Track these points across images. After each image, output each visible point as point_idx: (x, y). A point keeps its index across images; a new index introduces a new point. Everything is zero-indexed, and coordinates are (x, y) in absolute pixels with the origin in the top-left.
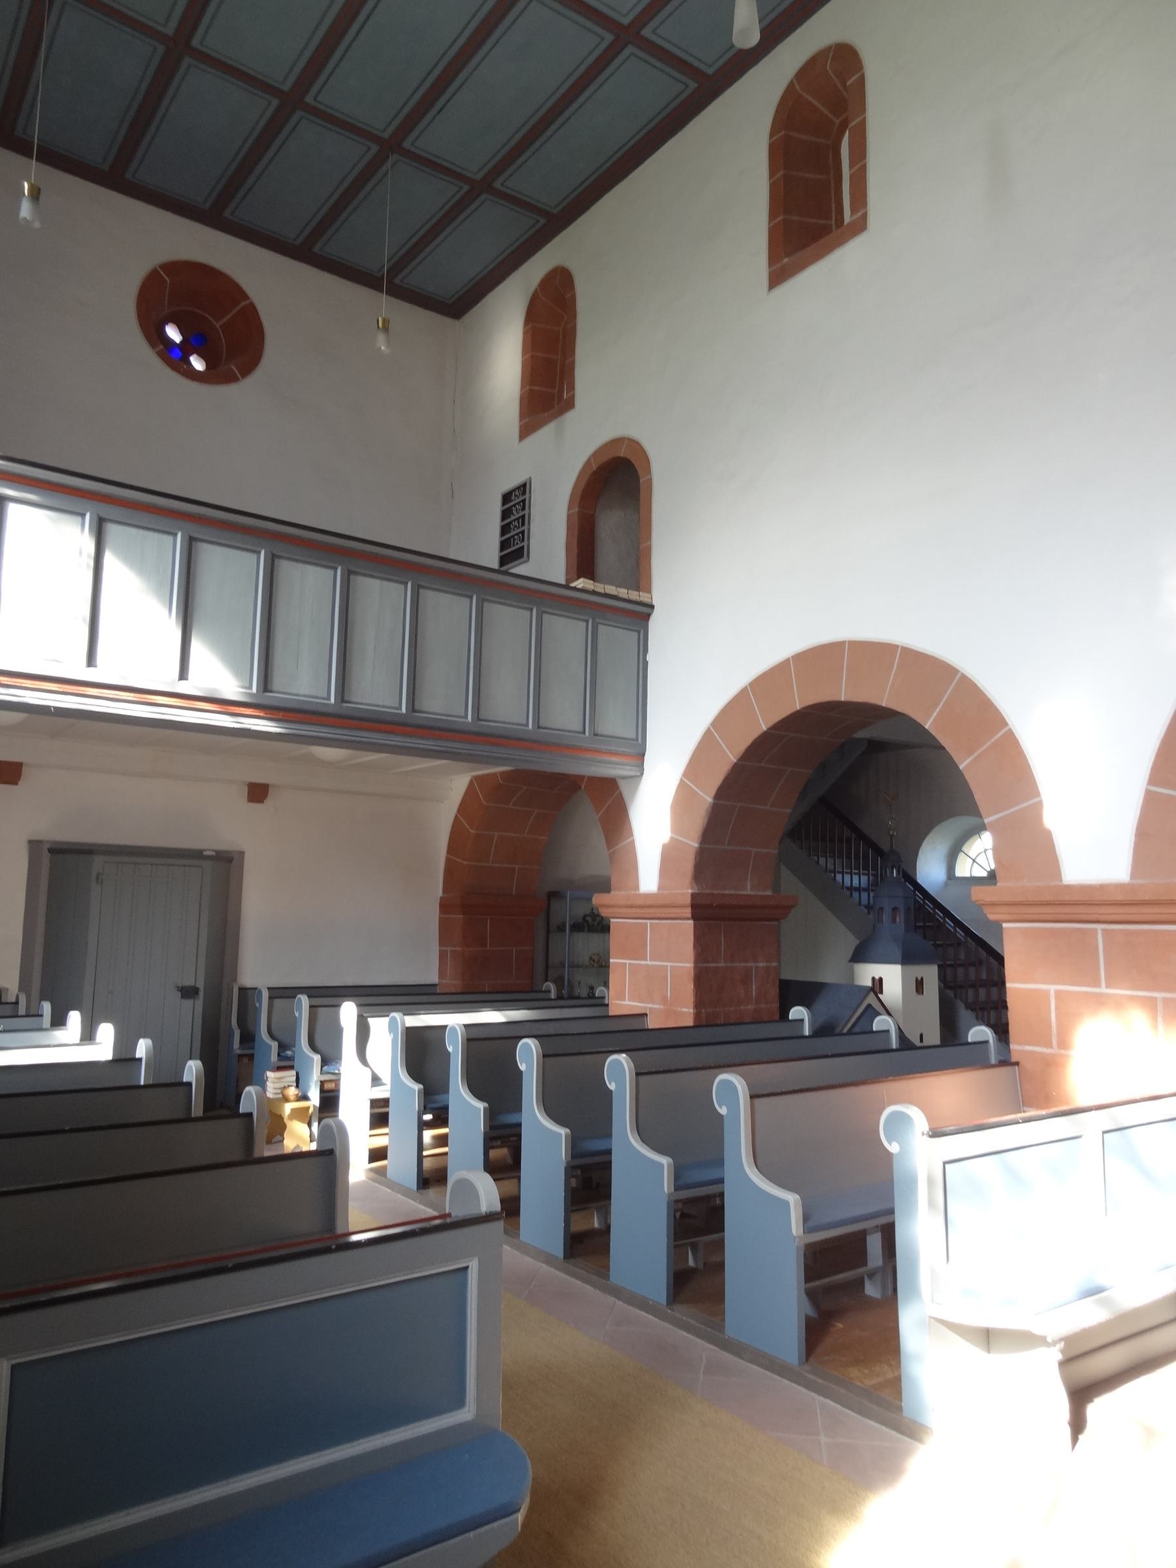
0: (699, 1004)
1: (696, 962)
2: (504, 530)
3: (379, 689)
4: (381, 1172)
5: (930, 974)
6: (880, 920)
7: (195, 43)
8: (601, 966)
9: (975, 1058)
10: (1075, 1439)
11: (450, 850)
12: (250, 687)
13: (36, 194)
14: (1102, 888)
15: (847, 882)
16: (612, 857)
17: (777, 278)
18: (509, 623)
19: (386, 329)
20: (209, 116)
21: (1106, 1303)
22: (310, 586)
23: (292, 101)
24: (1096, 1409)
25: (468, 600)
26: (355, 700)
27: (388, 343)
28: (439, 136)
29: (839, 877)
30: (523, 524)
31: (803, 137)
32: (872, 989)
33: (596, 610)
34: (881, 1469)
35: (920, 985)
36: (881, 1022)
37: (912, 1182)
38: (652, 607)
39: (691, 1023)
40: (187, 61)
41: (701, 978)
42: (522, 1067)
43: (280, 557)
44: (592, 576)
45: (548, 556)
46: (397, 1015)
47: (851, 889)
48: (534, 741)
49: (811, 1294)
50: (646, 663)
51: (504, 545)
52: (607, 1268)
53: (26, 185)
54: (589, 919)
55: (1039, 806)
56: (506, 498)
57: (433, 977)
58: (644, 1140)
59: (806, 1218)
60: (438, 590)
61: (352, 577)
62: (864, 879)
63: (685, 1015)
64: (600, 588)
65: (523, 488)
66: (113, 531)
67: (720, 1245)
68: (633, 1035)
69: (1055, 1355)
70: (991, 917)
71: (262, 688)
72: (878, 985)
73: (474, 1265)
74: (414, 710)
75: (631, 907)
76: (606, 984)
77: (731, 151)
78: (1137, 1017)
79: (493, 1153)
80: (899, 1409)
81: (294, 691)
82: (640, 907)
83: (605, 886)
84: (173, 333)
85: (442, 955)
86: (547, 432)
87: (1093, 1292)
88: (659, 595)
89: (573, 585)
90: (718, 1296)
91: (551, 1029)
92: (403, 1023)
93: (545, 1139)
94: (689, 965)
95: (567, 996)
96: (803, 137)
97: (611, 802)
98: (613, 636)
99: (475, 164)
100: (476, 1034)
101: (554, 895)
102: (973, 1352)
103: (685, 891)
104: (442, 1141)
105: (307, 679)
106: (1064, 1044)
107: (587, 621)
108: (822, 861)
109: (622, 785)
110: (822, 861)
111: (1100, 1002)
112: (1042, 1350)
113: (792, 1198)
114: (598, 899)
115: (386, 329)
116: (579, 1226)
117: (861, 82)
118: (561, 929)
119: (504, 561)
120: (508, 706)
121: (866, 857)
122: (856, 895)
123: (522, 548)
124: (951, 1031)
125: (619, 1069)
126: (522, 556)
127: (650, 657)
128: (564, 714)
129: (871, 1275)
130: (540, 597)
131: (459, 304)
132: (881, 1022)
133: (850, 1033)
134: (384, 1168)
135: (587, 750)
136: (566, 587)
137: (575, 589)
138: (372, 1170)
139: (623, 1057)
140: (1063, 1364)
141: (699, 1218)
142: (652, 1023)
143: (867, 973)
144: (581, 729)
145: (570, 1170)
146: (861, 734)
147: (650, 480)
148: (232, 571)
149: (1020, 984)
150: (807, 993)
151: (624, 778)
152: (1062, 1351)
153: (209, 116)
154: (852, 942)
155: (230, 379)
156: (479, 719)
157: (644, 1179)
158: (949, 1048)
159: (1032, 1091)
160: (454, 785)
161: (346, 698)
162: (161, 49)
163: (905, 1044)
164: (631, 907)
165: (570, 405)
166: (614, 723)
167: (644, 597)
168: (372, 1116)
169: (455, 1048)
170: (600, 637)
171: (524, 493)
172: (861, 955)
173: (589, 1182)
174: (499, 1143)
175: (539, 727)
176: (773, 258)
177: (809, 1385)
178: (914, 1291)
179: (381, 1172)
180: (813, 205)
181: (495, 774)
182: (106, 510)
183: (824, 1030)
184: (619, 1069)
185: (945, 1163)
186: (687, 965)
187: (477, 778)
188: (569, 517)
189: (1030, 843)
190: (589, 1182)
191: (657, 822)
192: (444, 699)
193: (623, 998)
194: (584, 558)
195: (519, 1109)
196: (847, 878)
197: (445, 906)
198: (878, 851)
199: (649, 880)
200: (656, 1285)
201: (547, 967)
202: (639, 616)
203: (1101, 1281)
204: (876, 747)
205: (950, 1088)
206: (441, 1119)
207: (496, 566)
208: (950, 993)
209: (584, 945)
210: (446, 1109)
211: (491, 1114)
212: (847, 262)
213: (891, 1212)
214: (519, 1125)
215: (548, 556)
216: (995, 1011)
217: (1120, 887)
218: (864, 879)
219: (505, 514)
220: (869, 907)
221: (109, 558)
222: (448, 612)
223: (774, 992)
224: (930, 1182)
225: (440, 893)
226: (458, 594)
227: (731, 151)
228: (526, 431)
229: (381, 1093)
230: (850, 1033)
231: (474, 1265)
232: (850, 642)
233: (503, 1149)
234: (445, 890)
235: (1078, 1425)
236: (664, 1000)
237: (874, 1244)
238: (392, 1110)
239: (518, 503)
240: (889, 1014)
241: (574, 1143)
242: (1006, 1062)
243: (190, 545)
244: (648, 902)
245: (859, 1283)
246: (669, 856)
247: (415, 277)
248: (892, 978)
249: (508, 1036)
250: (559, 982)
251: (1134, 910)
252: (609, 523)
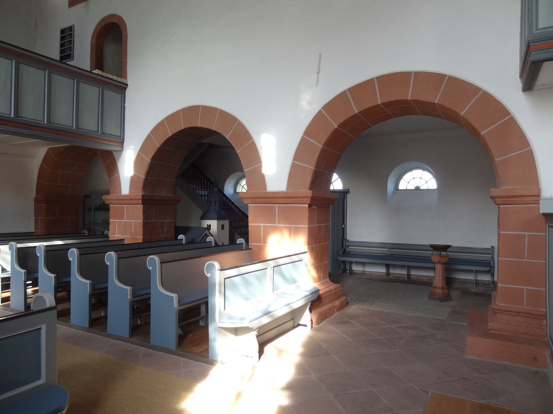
0: (144, 235)
1: (143, 220)
2: (62, 45)
4: (8, 306)
5: (226, 223)
6: (211, 205)
8: (107, 224)
9: (239, 248)
10: (260, 357)
11: (39, 177)
14: (278, 193)
15: (200, 193)
16: (110, 181)
18: (64, 85)
21: (270, 316)
24: (267, 348)
29: (198, 191)
30: (71, 44)
31: (513, 154)
32: (207, 228)
33: (103, 84)
34: (202, 375)
35: (223, 227)
36: (209, 239)
37: (214, 285)
38: (127, 85)
39: (139, 238)
41: (145, 226)
42: (71, 259)
44: (102, 70)
45: (82, 57)
46: (13, 243)
47: (201, 195)
49: (181, 327)
50: (124, 107)
51: (62, 52)
52: (106, 328)
54: (102, 206)
55: (261, 166)
57: (32, 229)
58: (121, 281)
59: (179, 302)
60: (29, 65)
62: (206, 192)
63: (139, 238)
64: (105, 74)
65: (71, 28)
67: (149, 316)
68: (119, 246)
69: (254, 333)
70: (245, 202)
72: (209, 227)
73: (44, 327)
74: (18, 116)
75: (118, 200)
76: (109, 230)
78: (286, 233)
79: (59, 295)
80: (208, 357)
82: (121, 200)
83: (108, 193)
85: (36, 221)
87: (267, 313)
88: (130, 80)
89: (93, 72)
90: (148, 332)
91: (85, 245)
92: (16, 246)
93: (80, 285)
94: (141, 221)
95: (92, 234)
96: (513, 154)
97: (110, 161)
98: (111, 96)
100: (49, 249)
101: (86, 197)
102: (231, 336)
103: (139, 194)
104: (36, 292)
106: (265, 242)
108: (192, 186)
109: (114, 153)
110: (192, 186)
111: (275, 229)
112: (252, 332)
113: (174, 296)
114: (104, 197)
116: (96, 315)
118: (90, 210)
119: (62, 58)
120: (63, 117)
121: (207, 185)
122: (203, 197)
124: (232, 241)
125: (111, 258)
126: (70, 58)
128: (89, 123)
129: (202, 319)
130: (77, 74)
132: (209, 239)
133: (199, 242)
134: (9, 304)
135: (100, 139)
136: (90, 72)
137: (94, 73)
138: (2, 306)
139: (112, 253)
140: (258, 336)
141: (141, 308)
142: (126, 242)
143: (206, 223)
145: (91, 296)
146: (205, 141)
147: (127, 34)
149: (252, 224)
150: (184, 230)
151: (116, 151)
152: (258, 332)
154: (202, 213)
157: (120, 293)
158: (232, 245)
159: (255, 256)
160: (39, 152)
163: (217, 245)
164: (118, 200)
166: (111, 129)
167: (123, 81)
168: (2, 285)
169: (41, 255)
170: (105, 95)
171: (71, 31)
172: (204, 217)
173: (99, 299)
174: (61, 289)
177: (179, 355)
178: (214, 320)
179: (8, 306)
181: (59, 147)
183: (190, 242)
184: (111, 258)
185: (225, 279)
186: (140, 221)
187: (50, 148)
188: (92, 44)
189: (258, 179)
190: (99, 299)
191: (128, 166)
192: (33, 111)
193: (115, 234)
194: (98, 61)
195: (69, 276)
196: (200, 192)
197: (37, 201)
198: (211, 183)
199: (125, 190)
200: (125, 331)
201: (84, 224)
202: (122, 88)
203: (270, 309)
204: (211, 146)
205: (230, 257)
206: (35, 283)
207: (58, 59)
208: (233, 230)
209: (100, 216)
210: (37, 278)
211: (57, 279)
213: (207, 297)
214: (70, 282)
215: (82, 57)
216: (245, 235)
217: (283, 192)
218: (206, 192)
219: (62, 39)
220: (207, 202)
222: (34, 77)
223: (173, 230)
224: (220, 284)
225: (34, 195)
226: (40, 69)
229: (5, 275)
230: (199, 242)
231: (44, 327)
232: (202, 106)
233: (63, 288)
234: (37, 193)
235: (261, 352)
236: (131, 234)
237: (203, 307)
238: (12, 283)
239: (68, 35)
240: (212, 236)
241: (93, 286)
242: (248, 249)
244: (125, 198)
245: (198, 322)
246: (133, 180)
248: (214, 224)
249: (65, 249)
250: (89, 230)
251: (287, 200)
252: (109, 50)
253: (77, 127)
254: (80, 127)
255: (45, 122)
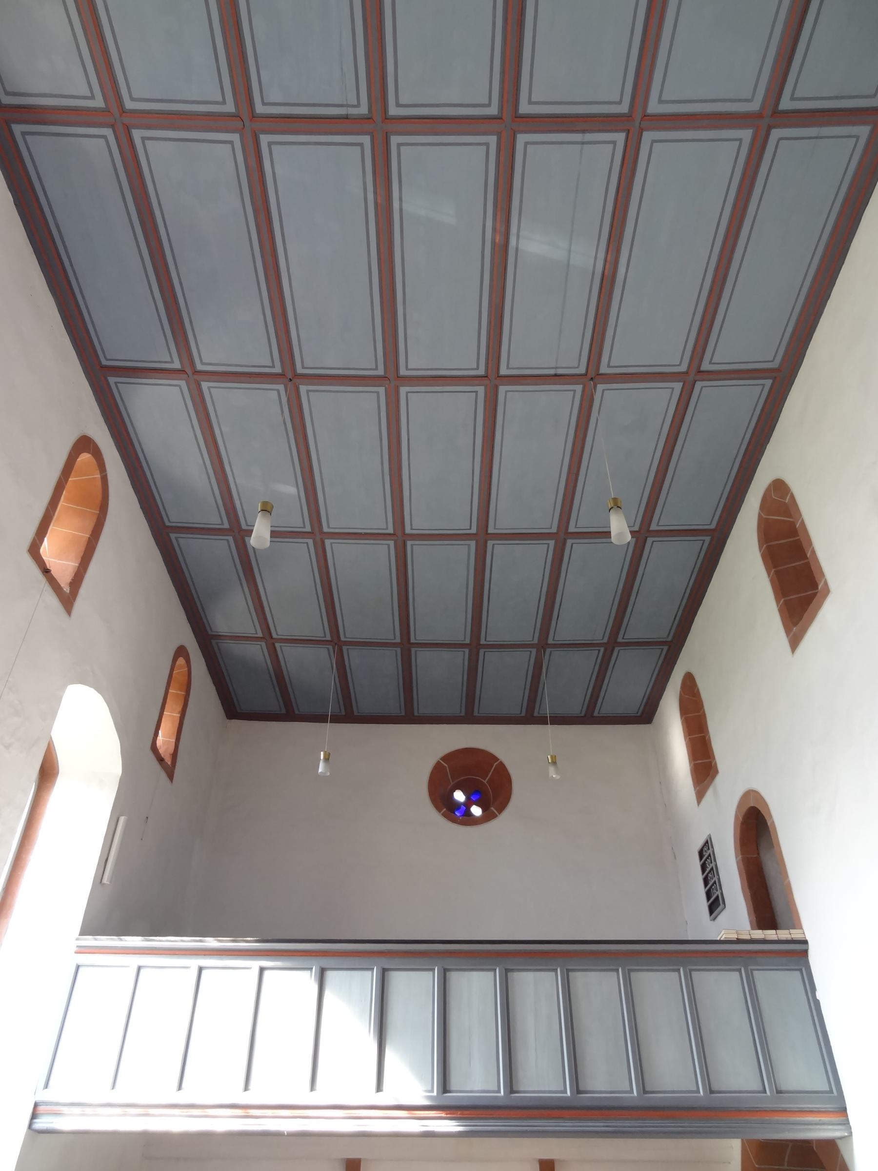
3: (543, 1076)
7: (413, 640)
12: (432, 1091)
13: (327, 759)
17: (795, 642)
19: (554, 763)
20: (439, 671)
22: (476, 988)
23: (475, 646)
25: (615, 974)
26: (521, 1089)
27: (557, 773)
28: (567, 627)
38: (805, 942)
40: (413, 650)
43: (450, 970)
48: (707, 1109)
50: (817, 1003)
53: (322, 753)
56: (701, 854)
61: (509, 974)
66: (332, 976)
71: (441, 1090)
74: (579, 1092)
77: (744, 564)
81: (468, 1089)
84: (459, 796)
86: (709, 793)
98: (773, 981)
99: (599, 632)
105: (478, 1077)
107: (740, 971)
109: (840, 1143)
115: (554, 763)
117: (792, 497)
123: (718, 897)
126: (719, 905)
127: (819, 995)
131: (647, 714)
144: (761, 1089)
148: (414, 988)
151: (841, 1138)
153: (439, 671)
155: (502, 808)
156: (645, 1092)
161: (515, 1089)
162: (399, 650)
165: (716, 772)
166: (798, 1073)
167: (795, 934)
175: (712, 1092)
176: (788, 630)
180: (798, 586)
182: (325, 962)
188: (738, 863)
192: (673, 1073)
202: (797, 954)
212: (829, 616)
221: (328, 994)
227: (744, 564)
228: (700, 795)
243: (384, 973)
247: (605, 707)
253: (578, 1090)
254: (715, 1087)
255: (635, 1093)
